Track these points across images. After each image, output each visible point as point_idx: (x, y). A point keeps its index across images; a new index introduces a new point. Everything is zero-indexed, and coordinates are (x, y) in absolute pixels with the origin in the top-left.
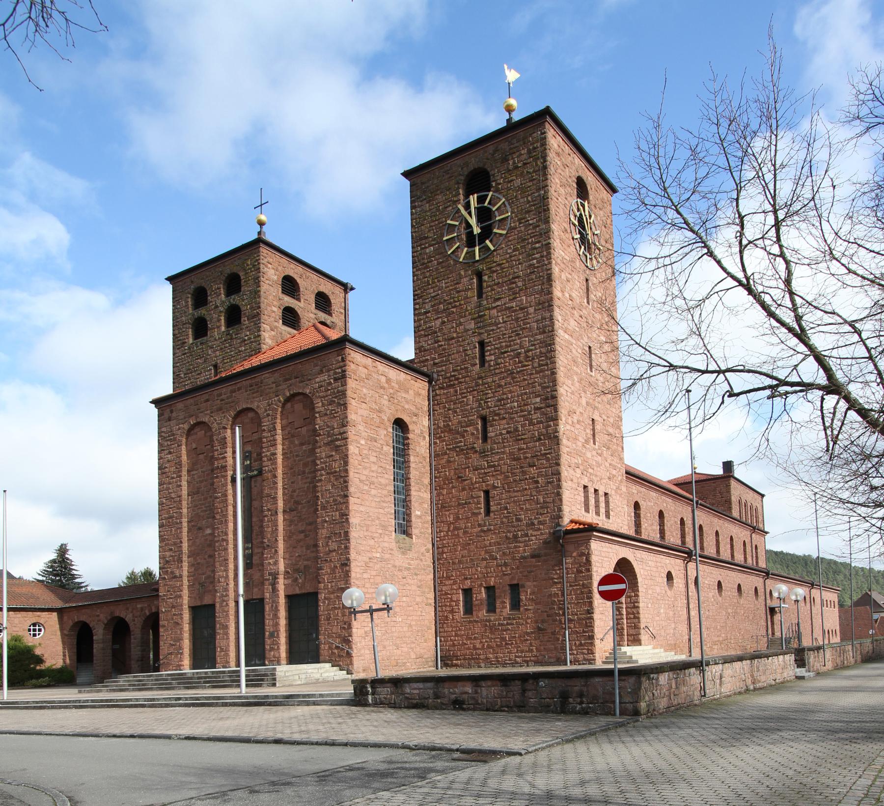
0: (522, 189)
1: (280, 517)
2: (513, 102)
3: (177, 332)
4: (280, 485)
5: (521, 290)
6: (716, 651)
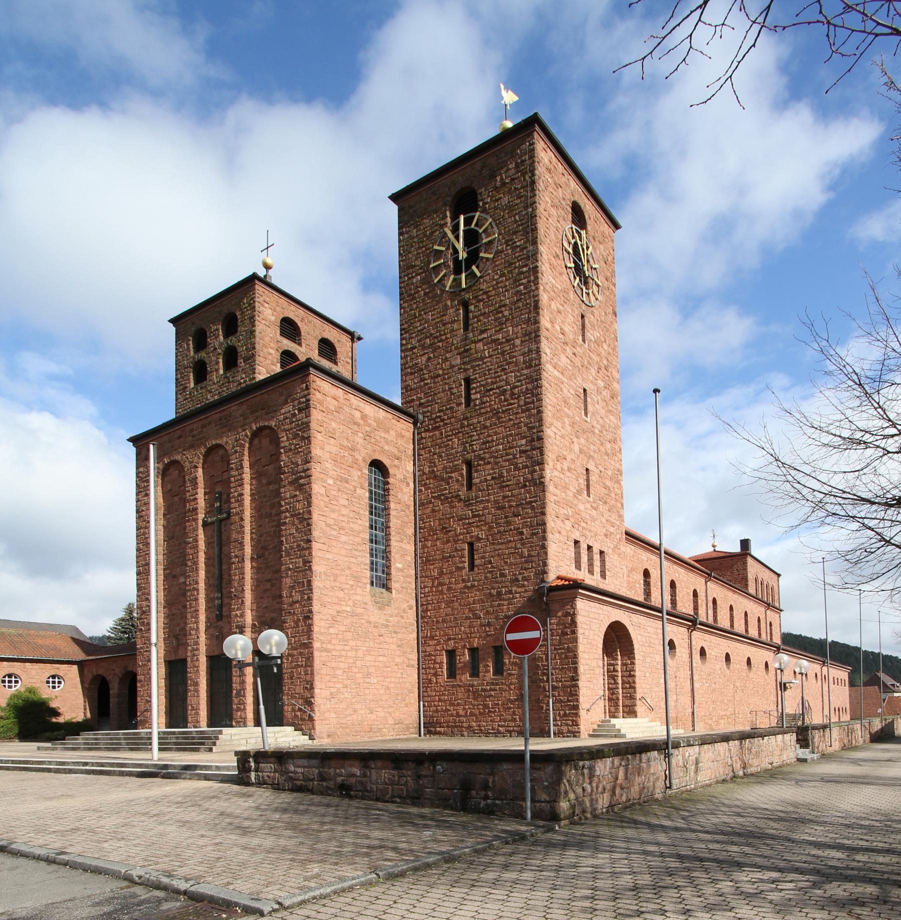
0: (510, 208)
1: (248, 565)
3: (179, 376)
4: (247, 529)
5: (507, 320)
6: (722, 725)
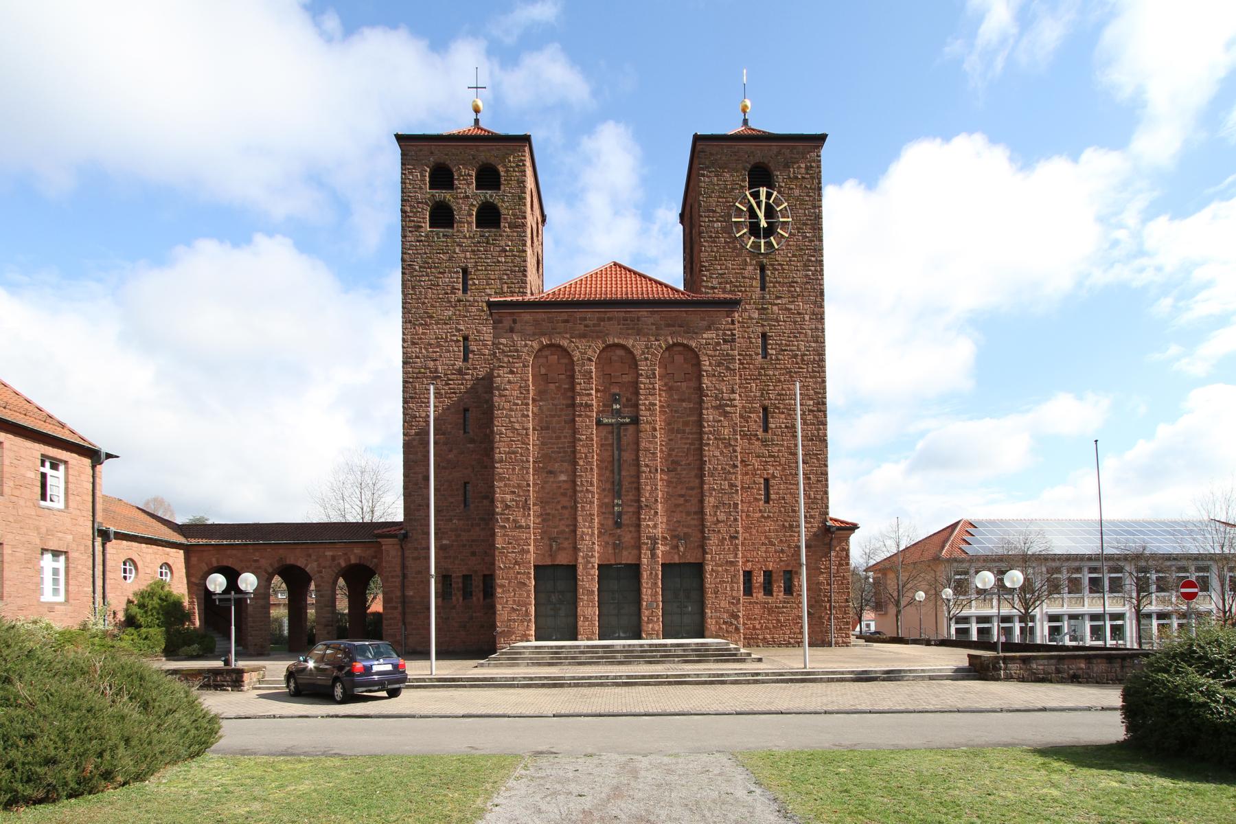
2: (748, 103)
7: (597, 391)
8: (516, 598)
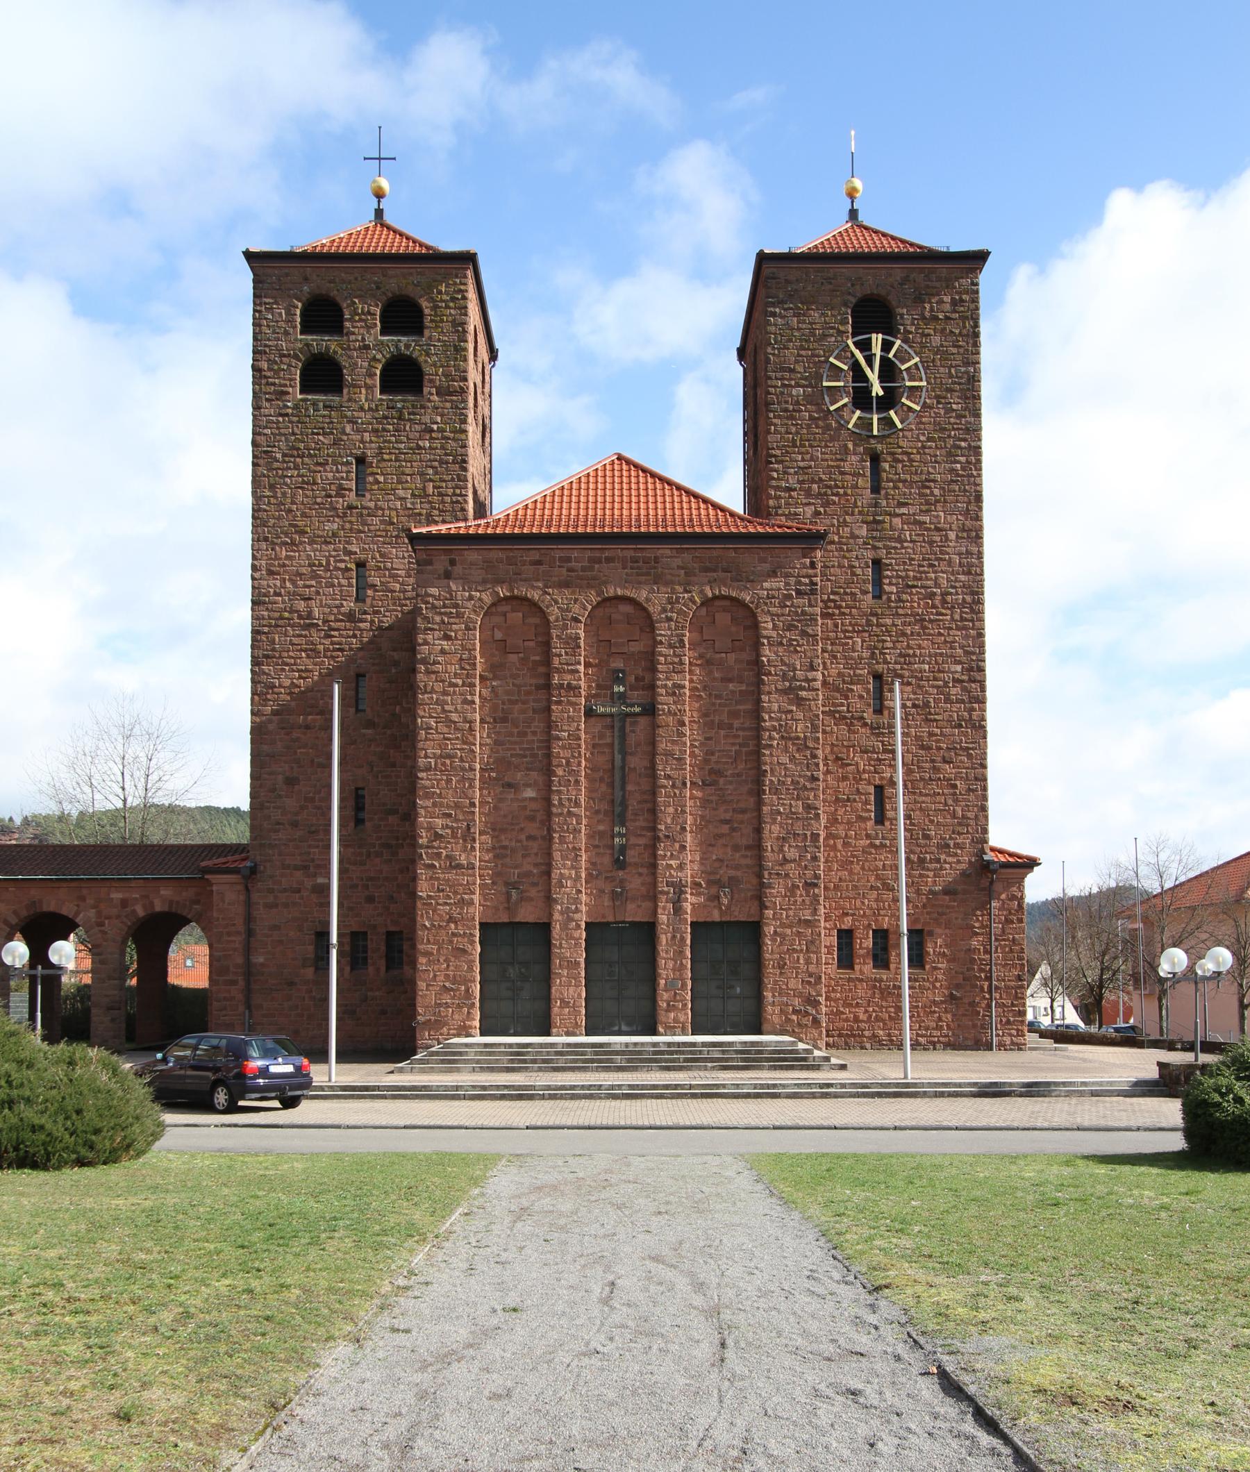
2: (858, 183)
5: (938, 501)
7: (587, 665)
8: (449, 969)
